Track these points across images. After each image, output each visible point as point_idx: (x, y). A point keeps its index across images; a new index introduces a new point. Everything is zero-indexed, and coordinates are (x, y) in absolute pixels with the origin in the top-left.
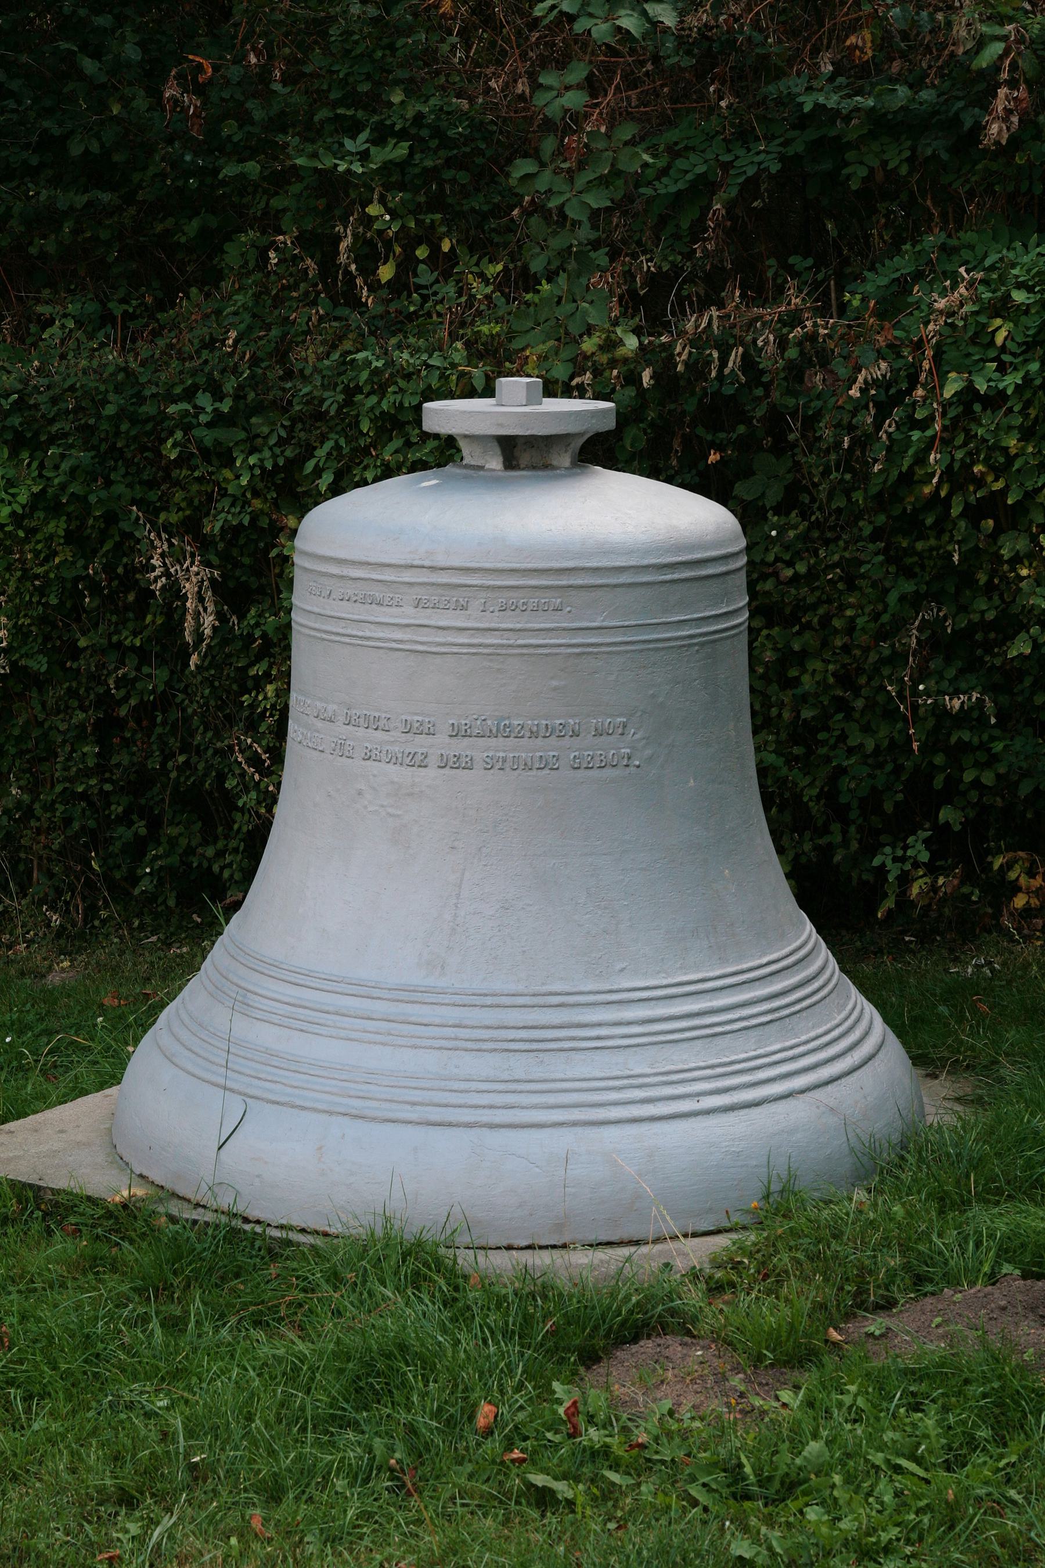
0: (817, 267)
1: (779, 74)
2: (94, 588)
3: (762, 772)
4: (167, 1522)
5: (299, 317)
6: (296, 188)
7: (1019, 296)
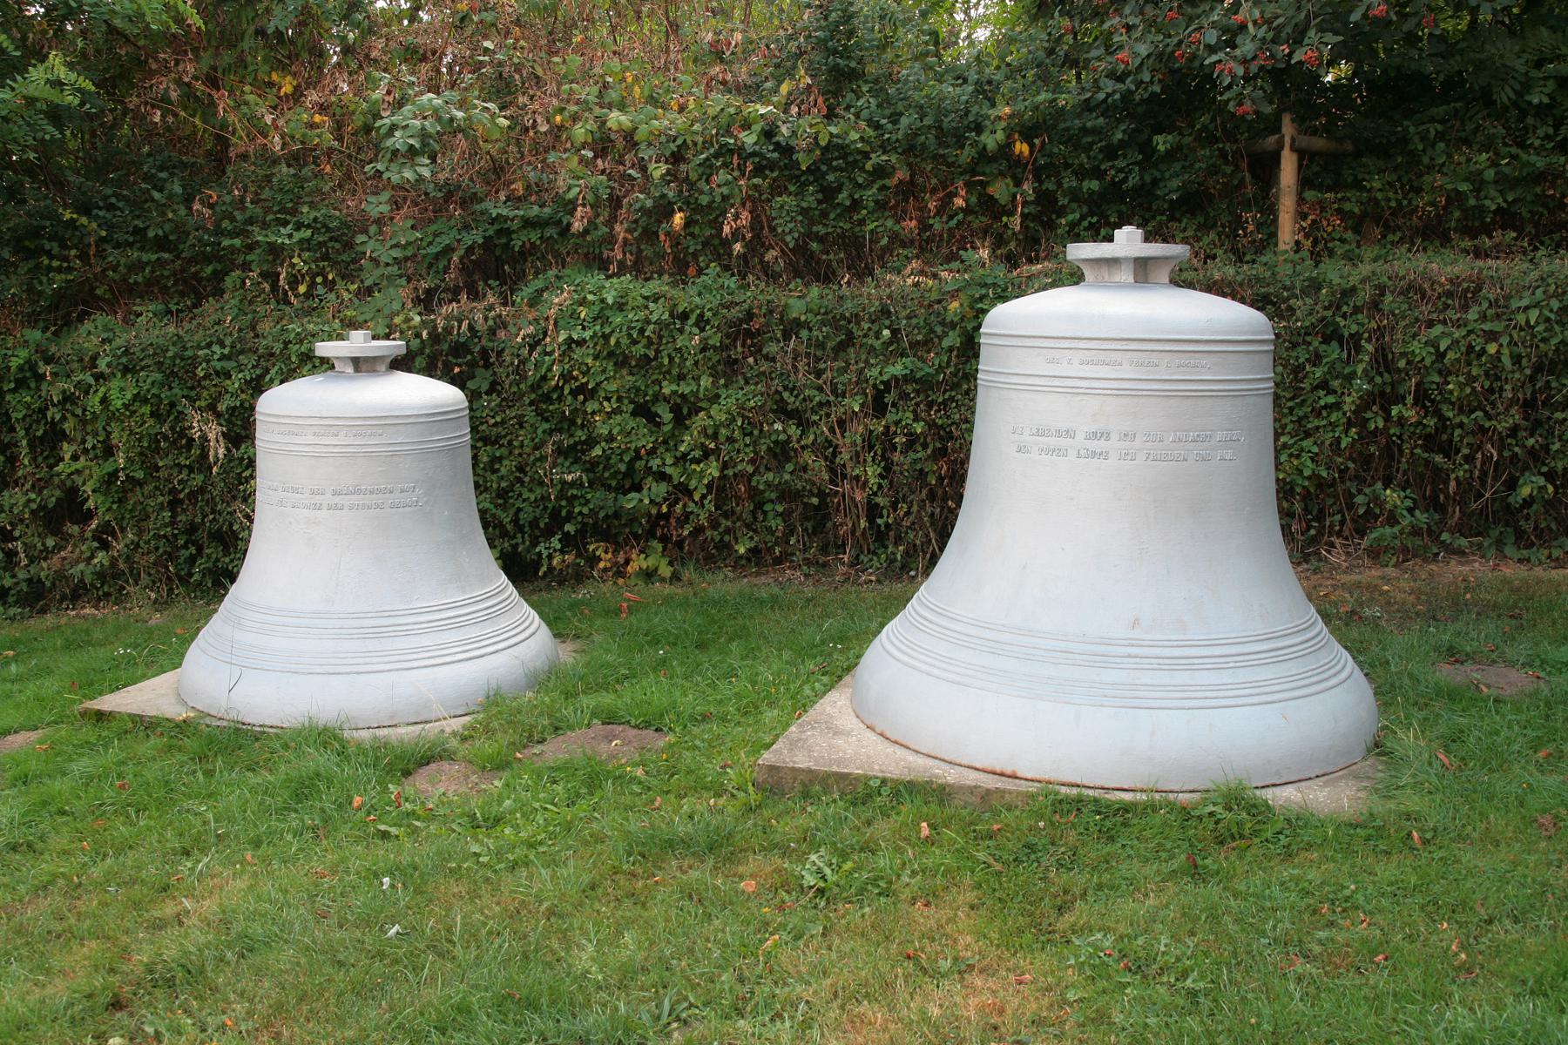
0: (501, 285)
1: (482, 200)
2: (166, 438)
3: (483, 513)
4: (206, 860)
5: (261, 309)
6: (258, 251)
7: (590, 297)
